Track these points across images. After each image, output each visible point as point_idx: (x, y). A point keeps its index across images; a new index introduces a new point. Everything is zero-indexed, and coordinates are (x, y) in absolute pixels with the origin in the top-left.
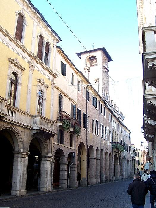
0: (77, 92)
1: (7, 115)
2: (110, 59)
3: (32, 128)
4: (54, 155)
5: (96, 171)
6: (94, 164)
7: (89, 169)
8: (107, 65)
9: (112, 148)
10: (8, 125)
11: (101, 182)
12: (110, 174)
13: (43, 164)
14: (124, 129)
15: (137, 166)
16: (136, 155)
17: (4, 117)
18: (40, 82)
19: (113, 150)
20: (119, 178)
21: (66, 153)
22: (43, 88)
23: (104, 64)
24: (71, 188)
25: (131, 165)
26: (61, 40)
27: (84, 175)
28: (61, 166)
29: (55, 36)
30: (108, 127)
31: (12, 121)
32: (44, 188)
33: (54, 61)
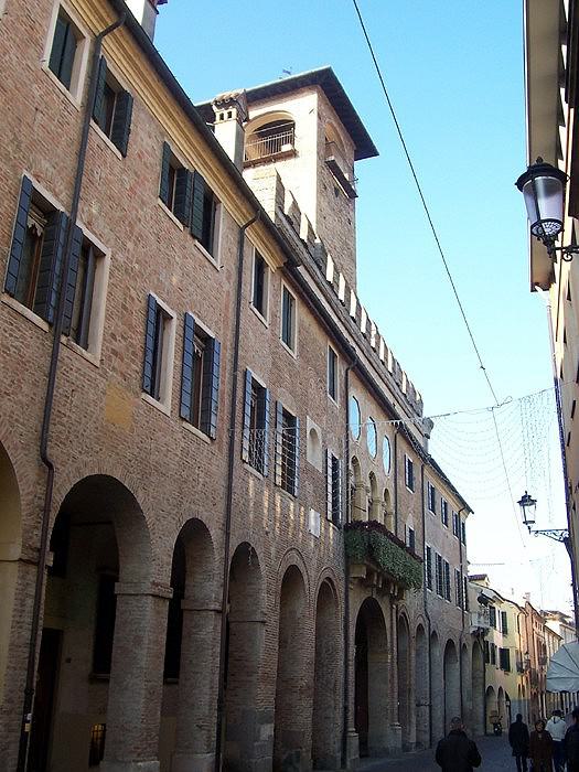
6: (148, 637)
9: (342, 560)
15: (496, 677)
16: (493, 624)
19: (347, 572)
25: (468, 670)
30: (310, 424)
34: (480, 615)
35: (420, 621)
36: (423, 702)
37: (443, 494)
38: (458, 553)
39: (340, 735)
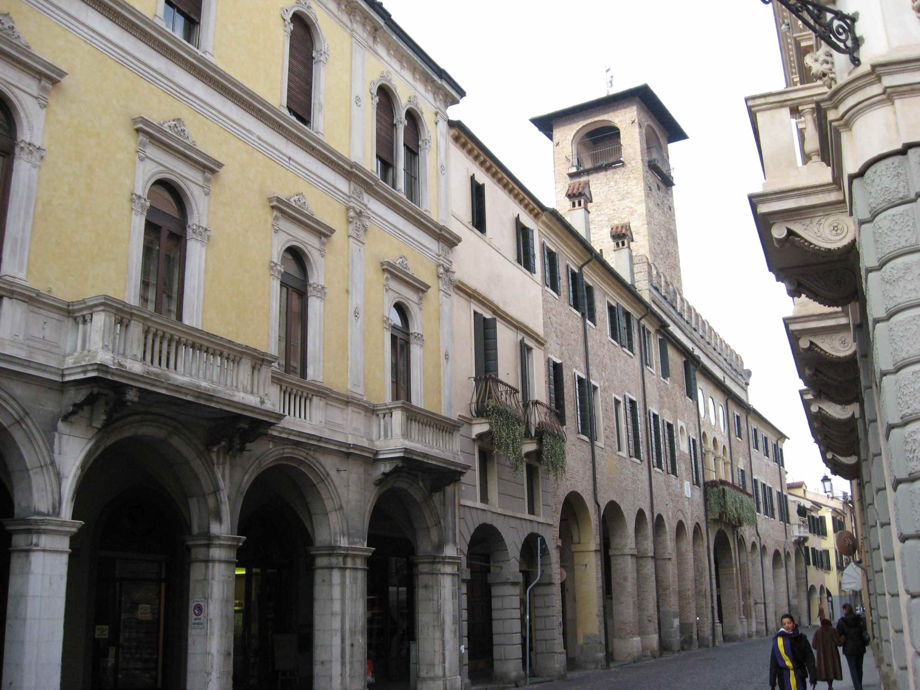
1: (280, 417)
2: (675, 133)
3: (377, 453)
4: (465, 549)
5: (640, 607)
7: (611, 598)
8: (666, 160)
10: (288, 451)
11: (664, 647)
12: (702, 618)
13: (426, 587)
17: (273, 424)
18: (393, 272)
19: (706, 515)
20: (740, 629)
21: (513, 542)
22: (409, 296)
24: (538, 676)
26: (462, 93)
27: (590, 623)
28: (496, 591)
29: (439, 82)
30: (680, 423)
31: (300, 434)
32: (433, 679)
33: (442, 184)
34: (799, 526)
35: (753, 539)
36: (759, 601)
37: (763, 432)
38: (778, 476)
39: (710, 625)
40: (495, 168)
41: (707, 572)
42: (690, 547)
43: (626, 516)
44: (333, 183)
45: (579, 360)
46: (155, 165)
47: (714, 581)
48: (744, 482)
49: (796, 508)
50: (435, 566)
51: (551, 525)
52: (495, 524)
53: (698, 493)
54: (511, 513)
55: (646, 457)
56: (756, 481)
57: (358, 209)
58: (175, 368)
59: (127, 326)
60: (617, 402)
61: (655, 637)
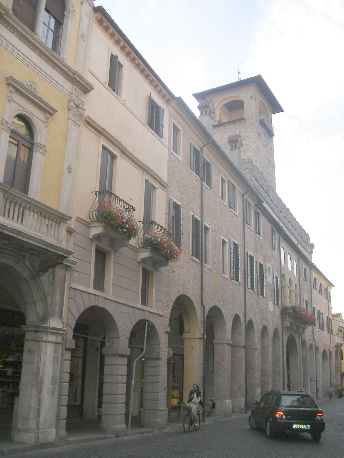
0: (170, 154)
2: (277, 108)
13: (29, 351)
14: (314, 275)
17: (66, 257)
19: (282, 324)
23: (263, 117)
28: (108, 360)
30: (268, 265)
35: (311, 342)
36: (313, 379)
37: (320, 280)
40: (133, 55)
41: (281, 359)
42: (271, 343)
43: (225, 318)
44: (35, 62)
45: (196, 206)
46: (17, 106)
47: (285, 365)
48: (307, 307)
49: (338, 327)
50: (38, 334)
51: (162, 316)
52: (107, 308)
53: (278, 311)
54: (123, 302)
55: (243, 282)
56: (314, 308)
57: (77, 102)
58: (22, 222)
59: (59, 224)
60: (224, 242)
61: (243, 399)
